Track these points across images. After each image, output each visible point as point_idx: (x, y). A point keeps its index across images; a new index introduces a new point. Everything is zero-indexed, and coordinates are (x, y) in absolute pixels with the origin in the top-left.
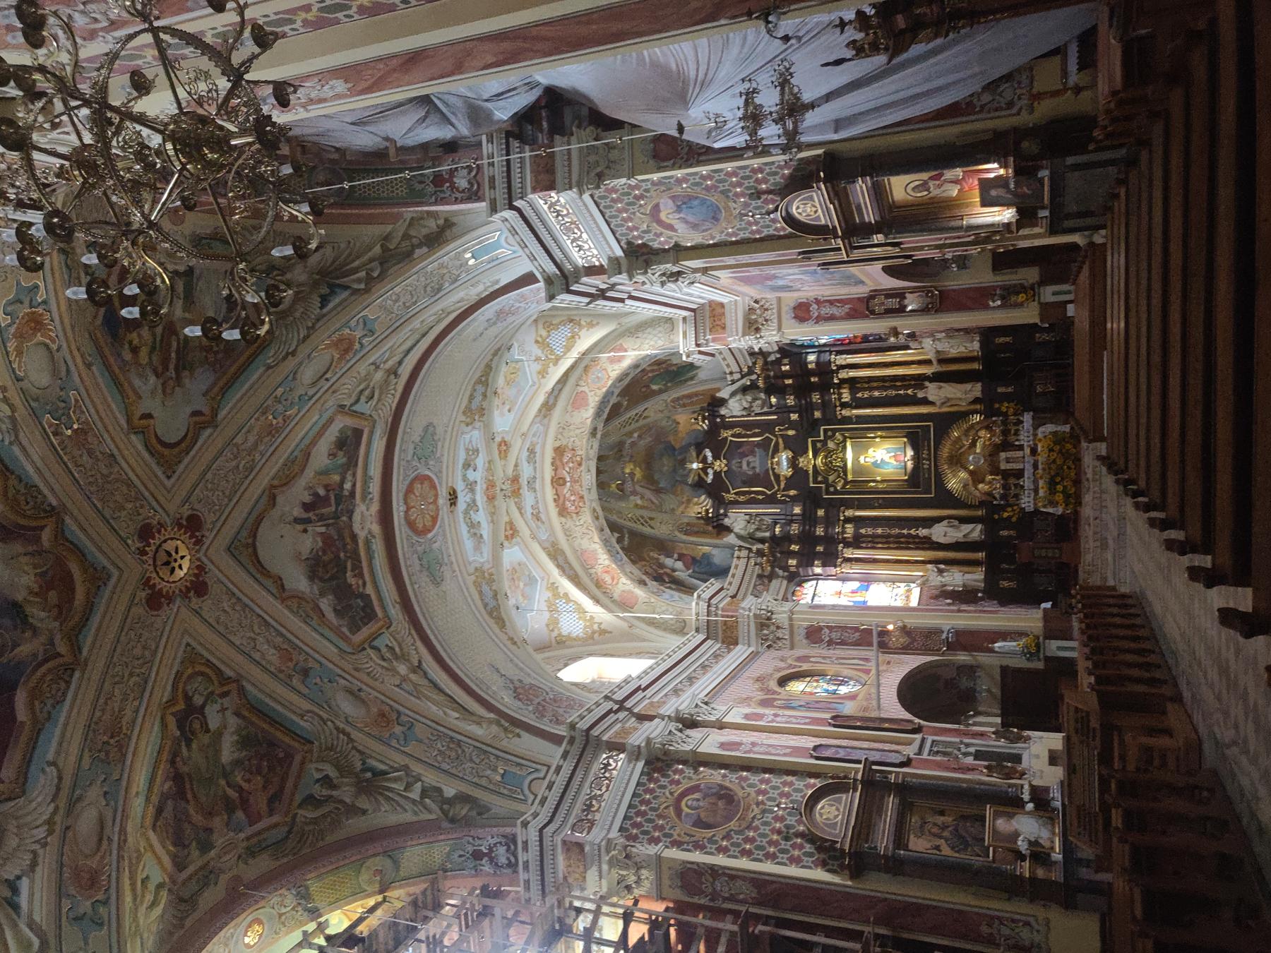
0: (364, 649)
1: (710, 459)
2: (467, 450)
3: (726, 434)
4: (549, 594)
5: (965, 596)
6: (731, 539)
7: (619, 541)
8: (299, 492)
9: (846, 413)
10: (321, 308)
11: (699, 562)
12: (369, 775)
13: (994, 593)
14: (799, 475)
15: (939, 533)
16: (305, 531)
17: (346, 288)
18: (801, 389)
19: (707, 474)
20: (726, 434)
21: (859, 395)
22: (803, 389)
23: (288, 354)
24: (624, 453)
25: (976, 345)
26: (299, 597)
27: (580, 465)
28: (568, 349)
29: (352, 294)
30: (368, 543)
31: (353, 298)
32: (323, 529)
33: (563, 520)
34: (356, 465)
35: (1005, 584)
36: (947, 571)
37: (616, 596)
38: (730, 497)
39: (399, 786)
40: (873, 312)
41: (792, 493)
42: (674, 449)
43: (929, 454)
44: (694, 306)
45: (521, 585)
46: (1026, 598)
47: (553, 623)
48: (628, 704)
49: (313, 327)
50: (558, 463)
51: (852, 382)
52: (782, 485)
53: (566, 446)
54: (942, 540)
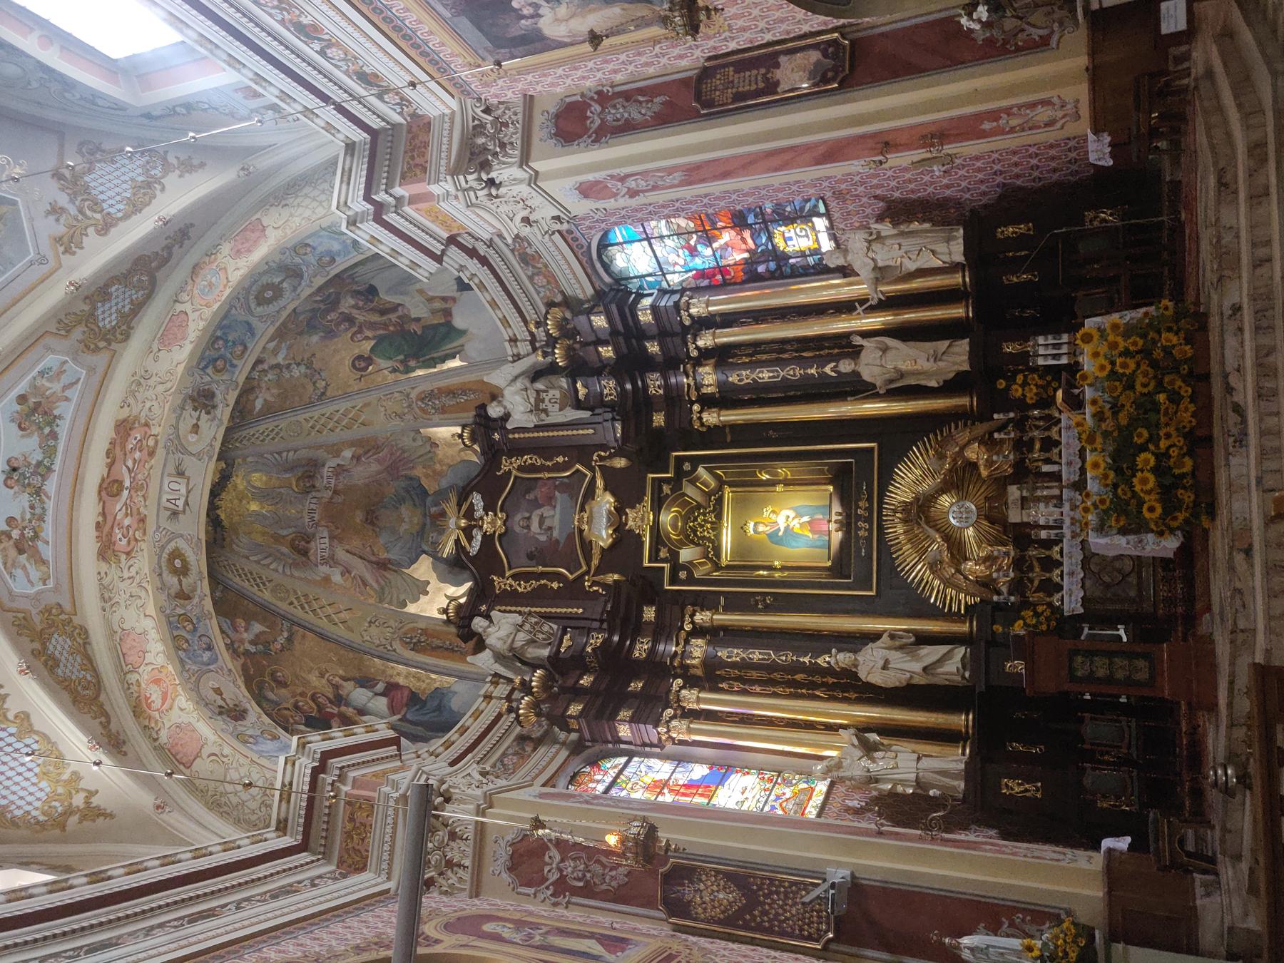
1: (479, 512)
5: (905, 810)
6: (484, 661)
9: (711, 418)
11: (424, 703)
13: (979, 807)
14: (625, 540)
15: (873, 665)
18: (647, 394)
19: (470, 538)
25: (956, 250)
27: (152, 454)
28: (135, 207)
33: (104, 567)
35: (1015, 787)
36: (888, 748)
37: (163, 737)
38: (501, 583)
42: (425, 493)
43: (870, 509)
44: (376, 123)
46: (1065, 824)
51: (721, 356)
52: (595, 562)
53: (136, 418)
54: (877, 678)
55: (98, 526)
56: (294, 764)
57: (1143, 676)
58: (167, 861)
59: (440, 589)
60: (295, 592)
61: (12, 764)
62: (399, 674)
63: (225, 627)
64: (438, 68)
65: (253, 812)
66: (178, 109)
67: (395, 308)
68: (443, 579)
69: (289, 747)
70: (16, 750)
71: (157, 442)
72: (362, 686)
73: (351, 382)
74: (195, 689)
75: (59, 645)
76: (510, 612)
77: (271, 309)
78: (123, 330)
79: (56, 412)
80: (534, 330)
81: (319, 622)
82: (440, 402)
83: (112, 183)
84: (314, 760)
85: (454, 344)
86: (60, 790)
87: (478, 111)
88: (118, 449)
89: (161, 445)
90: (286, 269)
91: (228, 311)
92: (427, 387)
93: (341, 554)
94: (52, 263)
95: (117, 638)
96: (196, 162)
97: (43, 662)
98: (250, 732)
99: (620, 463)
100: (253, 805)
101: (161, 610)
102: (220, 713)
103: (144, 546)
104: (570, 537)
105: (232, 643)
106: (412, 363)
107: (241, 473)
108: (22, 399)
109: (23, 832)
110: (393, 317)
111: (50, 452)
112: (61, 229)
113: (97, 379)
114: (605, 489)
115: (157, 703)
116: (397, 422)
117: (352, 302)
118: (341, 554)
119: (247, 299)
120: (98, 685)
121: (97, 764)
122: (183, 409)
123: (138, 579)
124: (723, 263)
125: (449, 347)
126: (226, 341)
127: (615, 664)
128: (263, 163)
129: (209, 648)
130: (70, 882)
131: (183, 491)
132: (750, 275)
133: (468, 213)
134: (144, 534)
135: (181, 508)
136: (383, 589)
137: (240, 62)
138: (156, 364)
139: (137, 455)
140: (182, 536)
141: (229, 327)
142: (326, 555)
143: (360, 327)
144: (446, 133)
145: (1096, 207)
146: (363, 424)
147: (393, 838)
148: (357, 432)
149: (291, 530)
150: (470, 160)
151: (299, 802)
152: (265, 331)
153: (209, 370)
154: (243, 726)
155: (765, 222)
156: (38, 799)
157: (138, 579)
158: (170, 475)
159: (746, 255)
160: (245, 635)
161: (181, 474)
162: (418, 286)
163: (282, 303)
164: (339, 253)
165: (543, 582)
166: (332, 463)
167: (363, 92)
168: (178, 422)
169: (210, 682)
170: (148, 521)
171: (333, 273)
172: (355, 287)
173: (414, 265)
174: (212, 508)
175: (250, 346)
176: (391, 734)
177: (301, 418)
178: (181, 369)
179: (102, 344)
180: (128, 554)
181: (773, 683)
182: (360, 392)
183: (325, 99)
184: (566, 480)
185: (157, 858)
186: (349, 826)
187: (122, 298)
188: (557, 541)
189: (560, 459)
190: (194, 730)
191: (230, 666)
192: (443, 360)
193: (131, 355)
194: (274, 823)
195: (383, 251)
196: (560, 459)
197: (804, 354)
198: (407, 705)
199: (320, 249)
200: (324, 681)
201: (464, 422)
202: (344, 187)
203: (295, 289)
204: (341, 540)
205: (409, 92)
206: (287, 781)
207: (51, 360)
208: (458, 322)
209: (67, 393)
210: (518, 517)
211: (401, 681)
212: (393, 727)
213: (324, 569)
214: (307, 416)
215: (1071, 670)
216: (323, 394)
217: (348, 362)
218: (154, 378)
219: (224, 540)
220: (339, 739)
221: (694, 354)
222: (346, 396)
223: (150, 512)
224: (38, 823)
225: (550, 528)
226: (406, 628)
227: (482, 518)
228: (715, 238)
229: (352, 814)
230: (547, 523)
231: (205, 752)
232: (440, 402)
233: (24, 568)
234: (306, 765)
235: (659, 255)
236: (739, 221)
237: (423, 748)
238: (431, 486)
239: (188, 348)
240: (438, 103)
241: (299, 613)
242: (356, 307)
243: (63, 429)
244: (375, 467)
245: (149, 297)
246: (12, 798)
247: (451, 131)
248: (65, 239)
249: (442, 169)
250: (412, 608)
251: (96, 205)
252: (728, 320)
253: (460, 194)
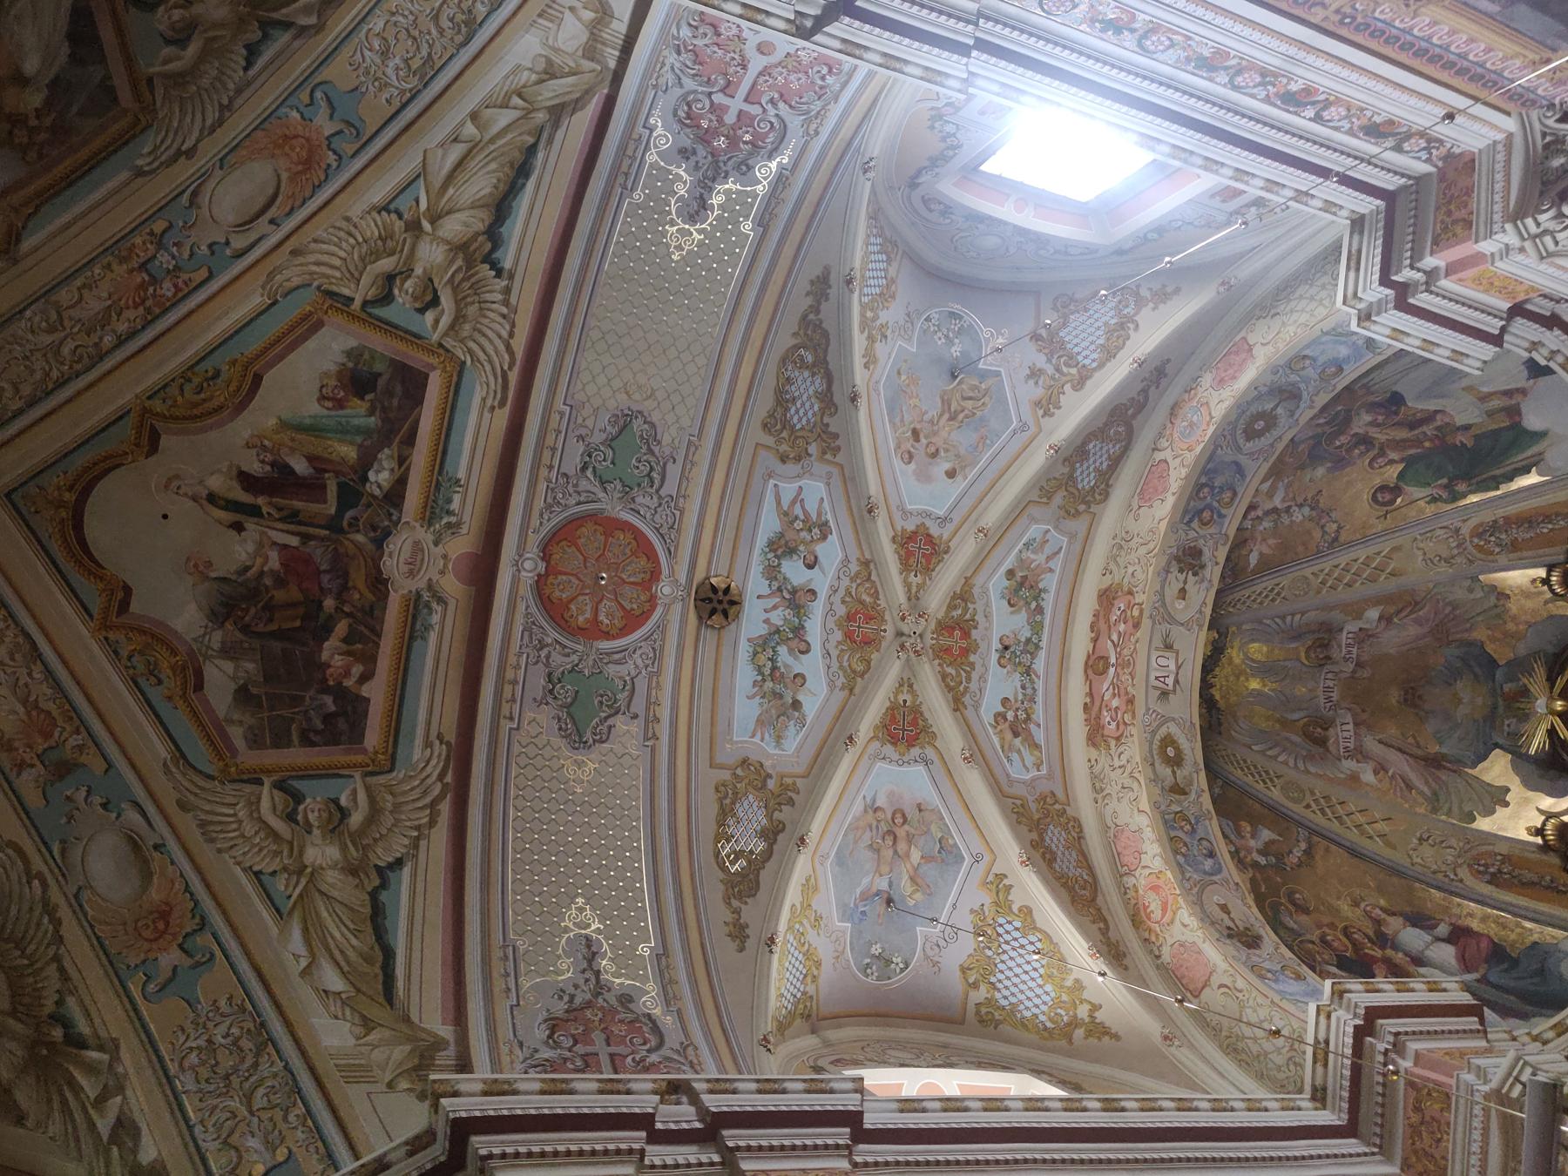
0: (260, 782)
2: (787, 517)
4: (987, 899)
8: (237, 442)
10: (246, 69)
11: (1515, 963)
12: (57, 1033)
16: (238, 527)
17: (286, 25)
23: (179, 153)
26: (156, 636)
27: (1137, 626)
29: (295, 38)
30: (416, 608)
31: (296, 44)
32: (294, 541)
33: (1094, 754)
34: (410, 440)
37: (1166, 956)
39: (90, 1088)
42: (1493, 663)
44: (1391, 183)
45: (916, 855)
47: (981, 970)
48: (733, 1137)
49: (229, 107)
50: (1102, 626)
53: (1120, 585)
55: (1086, 707)
56: (1329, 1017)
58: (1184, 1106)
59: (1527, 800)
60: (1313, 793)
61: (1020, 960)
62: (1471, 915)
63: (1227, 831)
64: (1480, 82)
65: (1279, 1068)
66: (1149, 236)
67: (1430, 417)
68: (1529, 784)
69: (1322, 993)
70: (1022, 947)
71: (1141, 611)
72: (1415, 925)
73: (1373, 521)
74: (1198, 903)
75: (1055, 837)
77: (1264, 441)
78: (1102, 490)
79: (1041, 586)
80: (273, 627)
81: (1348, 835)
82: (1514, 536)
83: (1083, 334)
84: (1355, 1016)
85: (1529, 452)
86: (1065, 997)
87: (1551, 122)
88: (1102, 622)
89: (1146, 614)
90: (1281, 390)
91: (1214, 452)
92: (1487, 516)
93: (1370, 743)
94: (1033, 429)
95: (1112, 834)
96: (1169, 290)
97: (1042, 856)
98: (1267, 965)
100: (1279, 1060)
101: (1156, 805)
102: (1230, 936)
103: (1134, 731)
105: (1237, 851)
106: (1461, 487)
107: (1236, 644)
108: (1010, 574)
109: (1033, 1037)
110: (1428, 430)
111: (1037, 628)
112: (1039, 392)
113: (1078, 547)
115: (1157, 915)
116: (1443, 568)
117: (1368, 418)
118: (1370, 743)
119: (1233, 435)
120: (1094, 885)
121: (1103, 975)
122: (1168, 572)
123: (1128, 770)
125: (1519, 458)
126: (1212, 488)
128: (1245, 272)
129: (1211, 854)
130: (1195, 1103)
131: (1173, 667)
133: (1543, 267)
134: (1134, 717)
135: (1171, 687)
136: (1435, 794)
137: (1217, 162)
138: (1140, 522)
139: (1122, 627)
140: (1174, 719)
141: (1215, 471)
142: (1352, 746)
143: (1381, 449)
144: (1498, 167)
146: (1392, 574)
147: (1485, 1152)
148: (1386, 585)
149: (1302, 714)
150: (1542, 193)
151: (1340, 1066)
152: (1256, 471)
153: (1195, 524)
154: (1256, 956)
156: (1045, 1003)
157: (1128, 770)
158: (1157, 649)
160: (1252, 843)
161: (1168, 647)
162: (1465, 383)
163: (1276, 433)
164: (1347, 359)
166: (1352, 627)
167: (1374, 150)
168: (1163, 587)
169: (1215, 897)
170: (1136, 702)
171: (1340, 387)
172: (1371, 398)
173: (1458, 355)
174: (1206, 685)
175: (1240, 491)
176: (1466, 998)
177: (1307, 572)
178: (1163, 526)
179: (1082, 507)
180: (1117, 739)
182: (1387, 532)
183: (1324, 173)
185: (1172, 1100)
186: (1415, 1118)
187: (1100, 454)
190: (1199, 952)
191: (1237, 879)
192: (1510, 478)
193: (1111, 516)
194: (1308, 1088)
195: (1411, 345)
198: (1487, 961)
199: (1321, 359)
200: (1358, 912)
201: (1549, 560)
202: (1352, 274)
203: (1292, 414)
204: (1370, 728)
205: (1444, 130)
206: (1322, 1037)
207: (1035, 531)
208: (1532, 422)
209: (1051, 564)
211: (1475, 925)
212: (1466, 987)
213: (1349, 765)
214: (1316, 569)
216: (1336, 539)
217: (1366, 497)
218: (1136, 539)
219: (1220, 724)
220: (1388, 994)
222: (1365, 540)
223: (1139, 693)
224: (1046, 1029)
226: (1474, 852)
229: (1418, 1101)
231: (1215, 981)
232: (1514, 536)
233: (1019, 752)
234: (1344, 1023)
237: (1521, 1029)
238: (1502, 654)
239: (1170, 500)
240: (1485, 130)
241: (1319, 819)
242: (1374, 424)
243: (1048, 603)
244: (1413, 631)
245: (1126, 450)
246: (1022, 997)
247: (1508, 162)
248: (1044, 402)
249: (1497, 217)
250: (1483, 824)
251: (1071, 359)
253: (1528, 245)
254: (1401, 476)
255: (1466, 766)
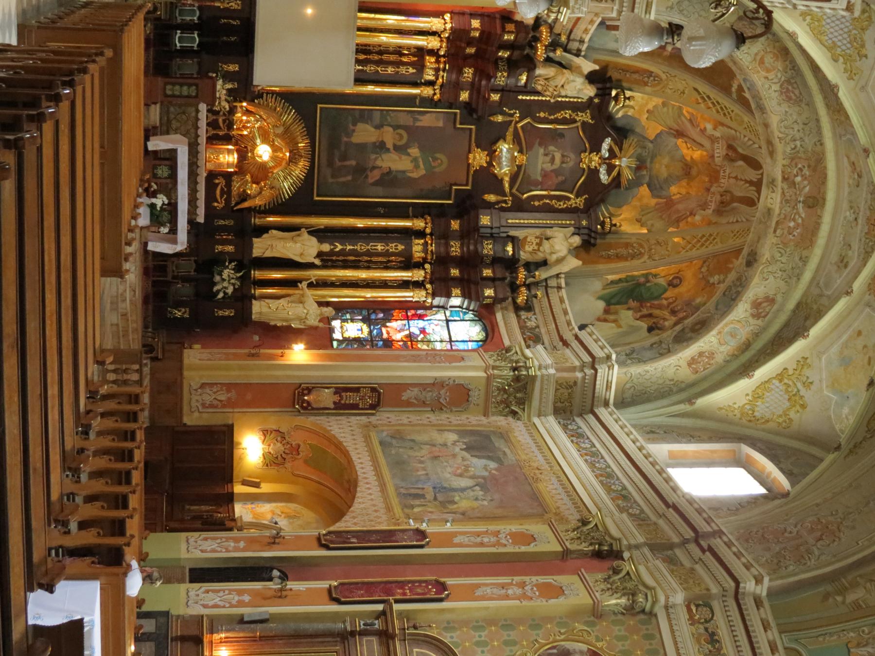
1: (603, 171)
3: (578, 202)
6: (588, 67)
7: (740, 89)
9: (419, 224)
14: (489, 145)
19: (611, 150)
20: (578, 202)
21: (401, 247)
22: (471, 262)
24: (718, 197)
28: (765, 384)
38: (585, 117)
40: (374, 390)
41: (500, 118)
44: (591, 418)
51: (408, 264)
52: (511, 129)
57: (169, 87)
67: (642, 317)
76: (575, 98)
99: (491, 198)
104: (530, 147)
106: (642, 280)
110: (645, 311)
112: (807, 372)
114: (502, 180)
116: (661, 239)
124: (405, 322)
127: (485, 63)
132: (388, 310)
136: (679, 117)
143: (668, 306)
145: (182, 319)
155: (372, 341)
159: (388, 324)
165: (552, 117)
166: (709, 212)
181: (380, 53)
184: (533, 188)
188: (540, 145)
189: (537, 203)
196: (537, 203)
197: (353, 258)
208: (601, 305)
210: (571, 164)
213: (717, 134)
214: (716, 247)
215: (197, 89)
221: (427, 266)
225: (546, 155)
226: (661, 86)
227: (600, 165)
228: (406, 336)
230: (548, 159)
235: (447, 332)
236: (388, 343)
242: (665, 319)
252: (405, 285)
254: (666, 290)
255: (667, 132)
